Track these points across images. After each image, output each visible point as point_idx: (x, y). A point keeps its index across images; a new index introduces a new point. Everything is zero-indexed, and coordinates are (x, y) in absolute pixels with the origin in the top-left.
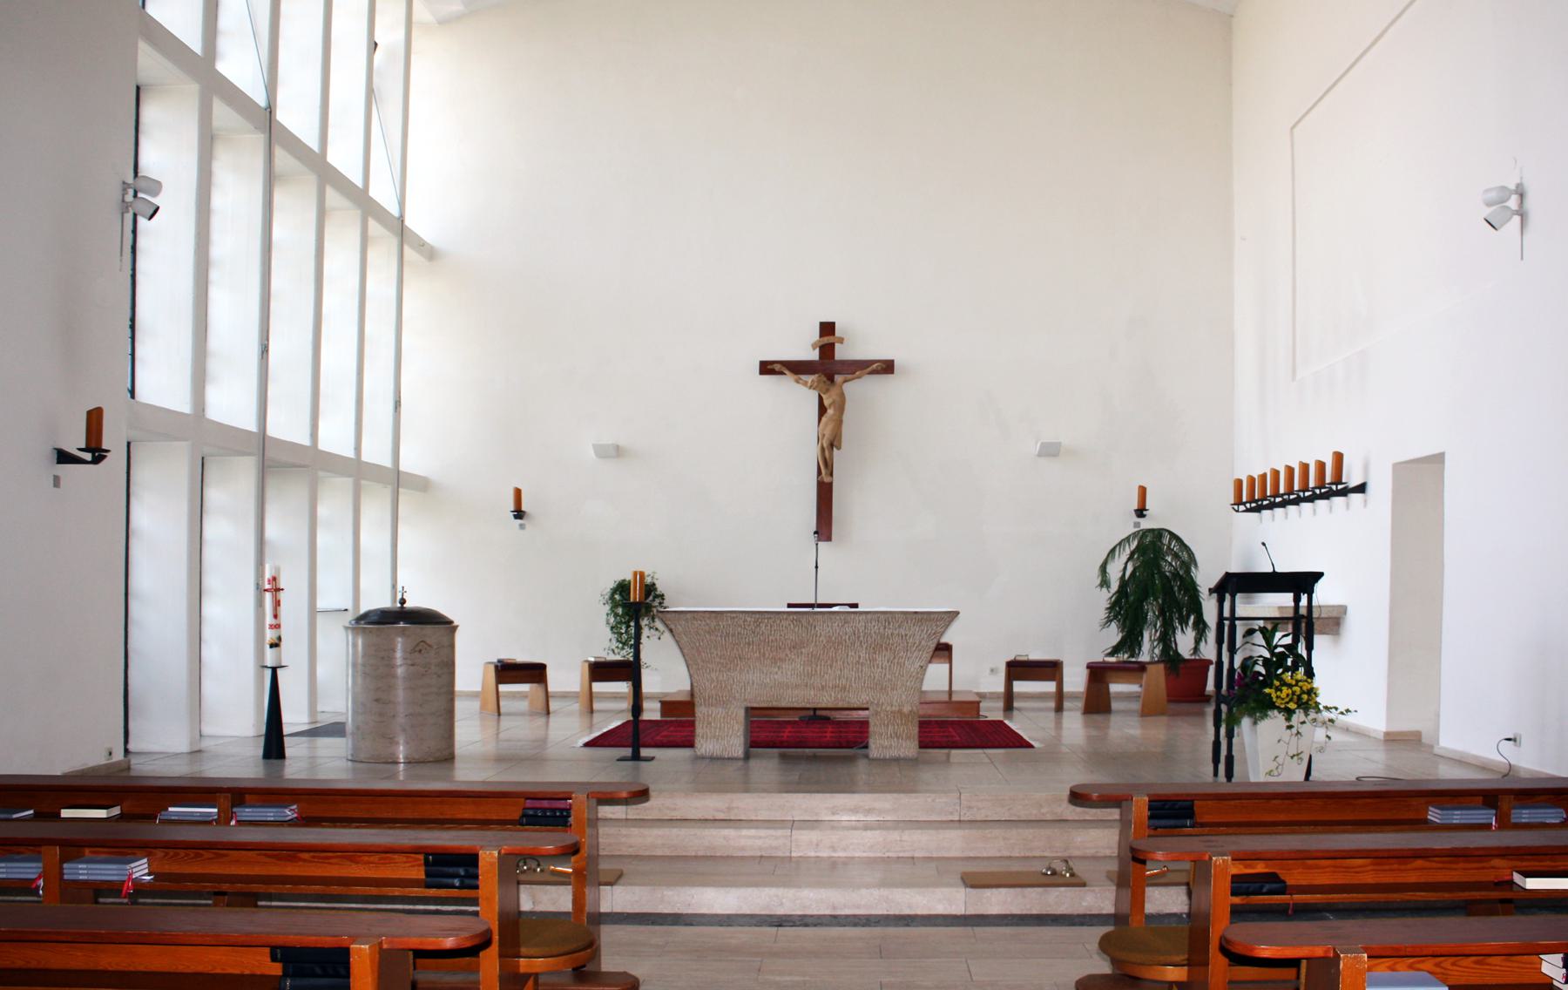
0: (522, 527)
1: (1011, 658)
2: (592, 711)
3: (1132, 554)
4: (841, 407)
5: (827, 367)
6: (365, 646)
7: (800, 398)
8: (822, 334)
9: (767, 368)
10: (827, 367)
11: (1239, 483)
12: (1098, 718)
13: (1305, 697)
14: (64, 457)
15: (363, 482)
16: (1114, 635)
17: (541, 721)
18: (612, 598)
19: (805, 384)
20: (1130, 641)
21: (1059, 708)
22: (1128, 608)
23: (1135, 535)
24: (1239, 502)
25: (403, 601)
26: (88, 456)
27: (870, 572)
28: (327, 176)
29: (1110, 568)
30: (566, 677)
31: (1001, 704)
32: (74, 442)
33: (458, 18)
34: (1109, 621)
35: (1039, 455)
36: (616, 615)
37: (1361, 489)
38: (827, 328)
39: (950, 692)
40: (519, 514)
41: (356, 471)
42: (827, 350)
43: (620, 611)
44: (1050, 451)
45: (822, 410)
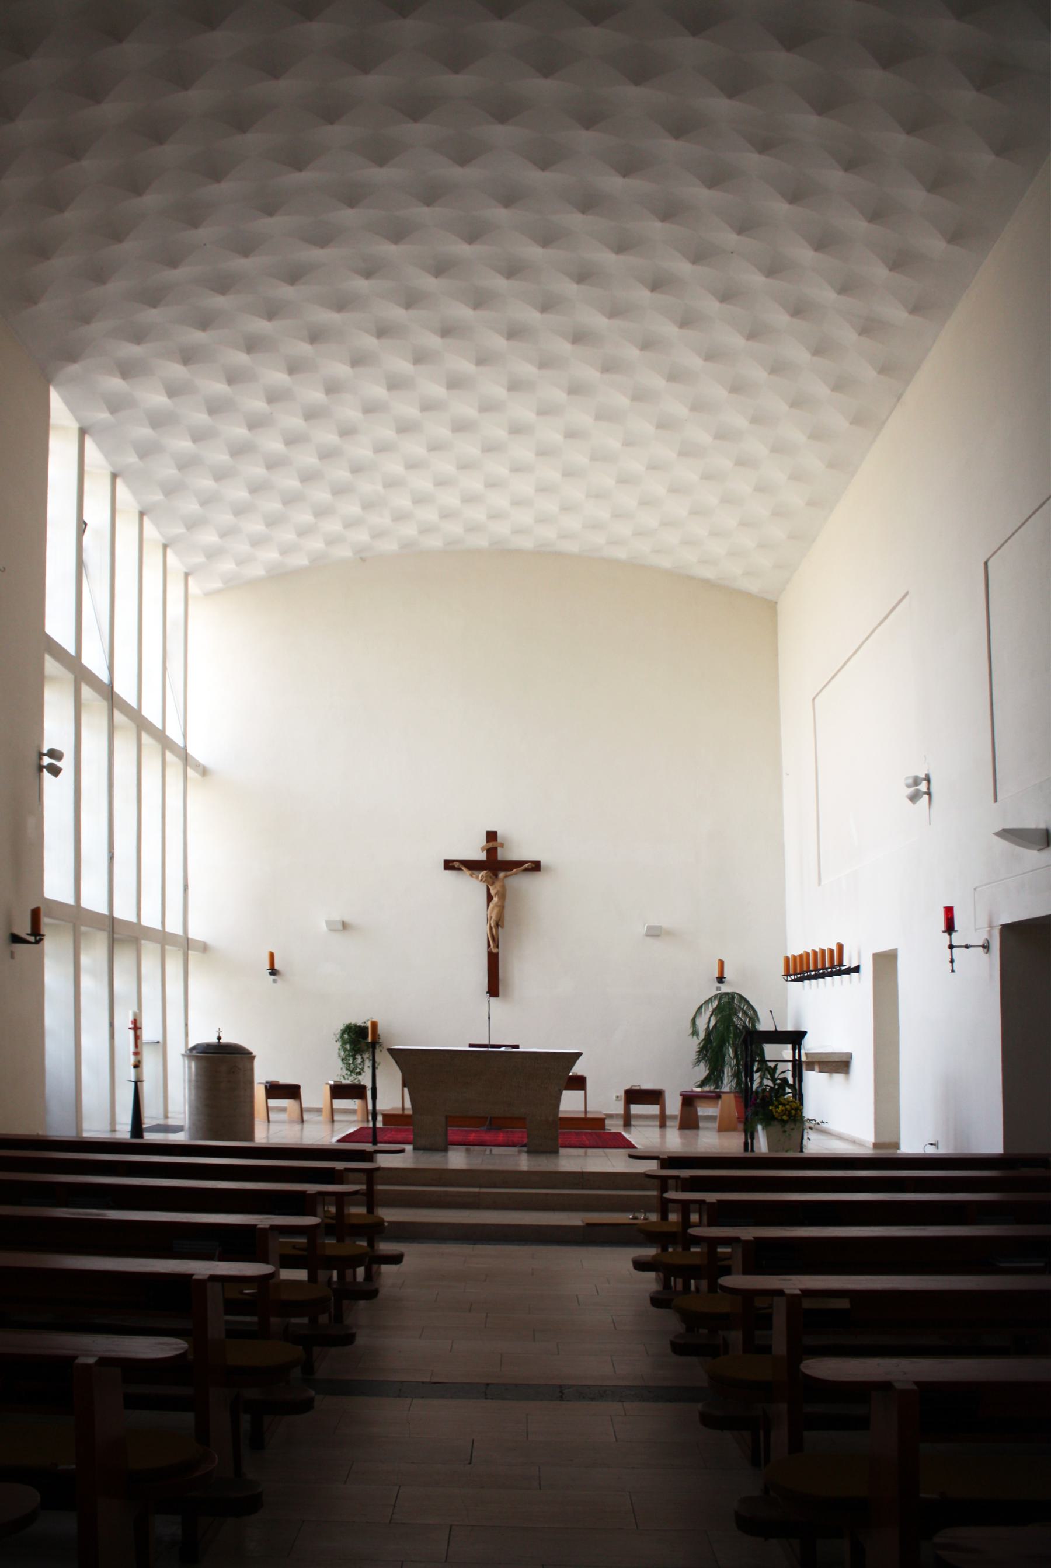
0: (275, 981)
1: (627, 1087)
2: (333, 1121)
3: (714, 1010)
4: (503, 896)
5: (495, 865)
6: (197, 1068)
7: (471, 889)
8: (488, 841)
9: (449, 865)
10: (495, 865)
11: (787, 959)
12: (687, 1132)
13: (793, 1112)
14: (16, 939)
15: (167, 947)
16: (703, 1071)
17: (298, 1127)
18: (342, 1037)
19: (477, 877)
20: (714, 1076)
21: (663, 1125)
22: (711, 1051)
23: (715, 996)
24: (788, 974)
25: (219, 1038)
26: (32, 939)
27: (523, 1026)
28: (142, 724)
29: (698, 1022)
30: (315, 1095)
31: (621, 1122)
32: (23, 929)
33: (218, 592)
34: (699, 1061)
35: (647, 935)
36: (345, 1050)
37: (857, 969)
38: (492, 836)
39: (586, 1112)
40: (273, 972)
41: (163, 938)
42: (491, 852)
43: (348, 1047)
44: (655, 933)
45: (490, 898)
